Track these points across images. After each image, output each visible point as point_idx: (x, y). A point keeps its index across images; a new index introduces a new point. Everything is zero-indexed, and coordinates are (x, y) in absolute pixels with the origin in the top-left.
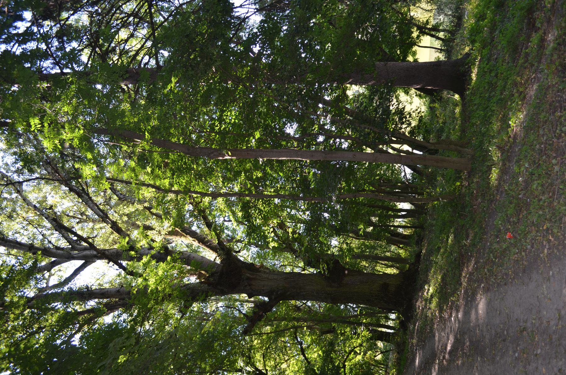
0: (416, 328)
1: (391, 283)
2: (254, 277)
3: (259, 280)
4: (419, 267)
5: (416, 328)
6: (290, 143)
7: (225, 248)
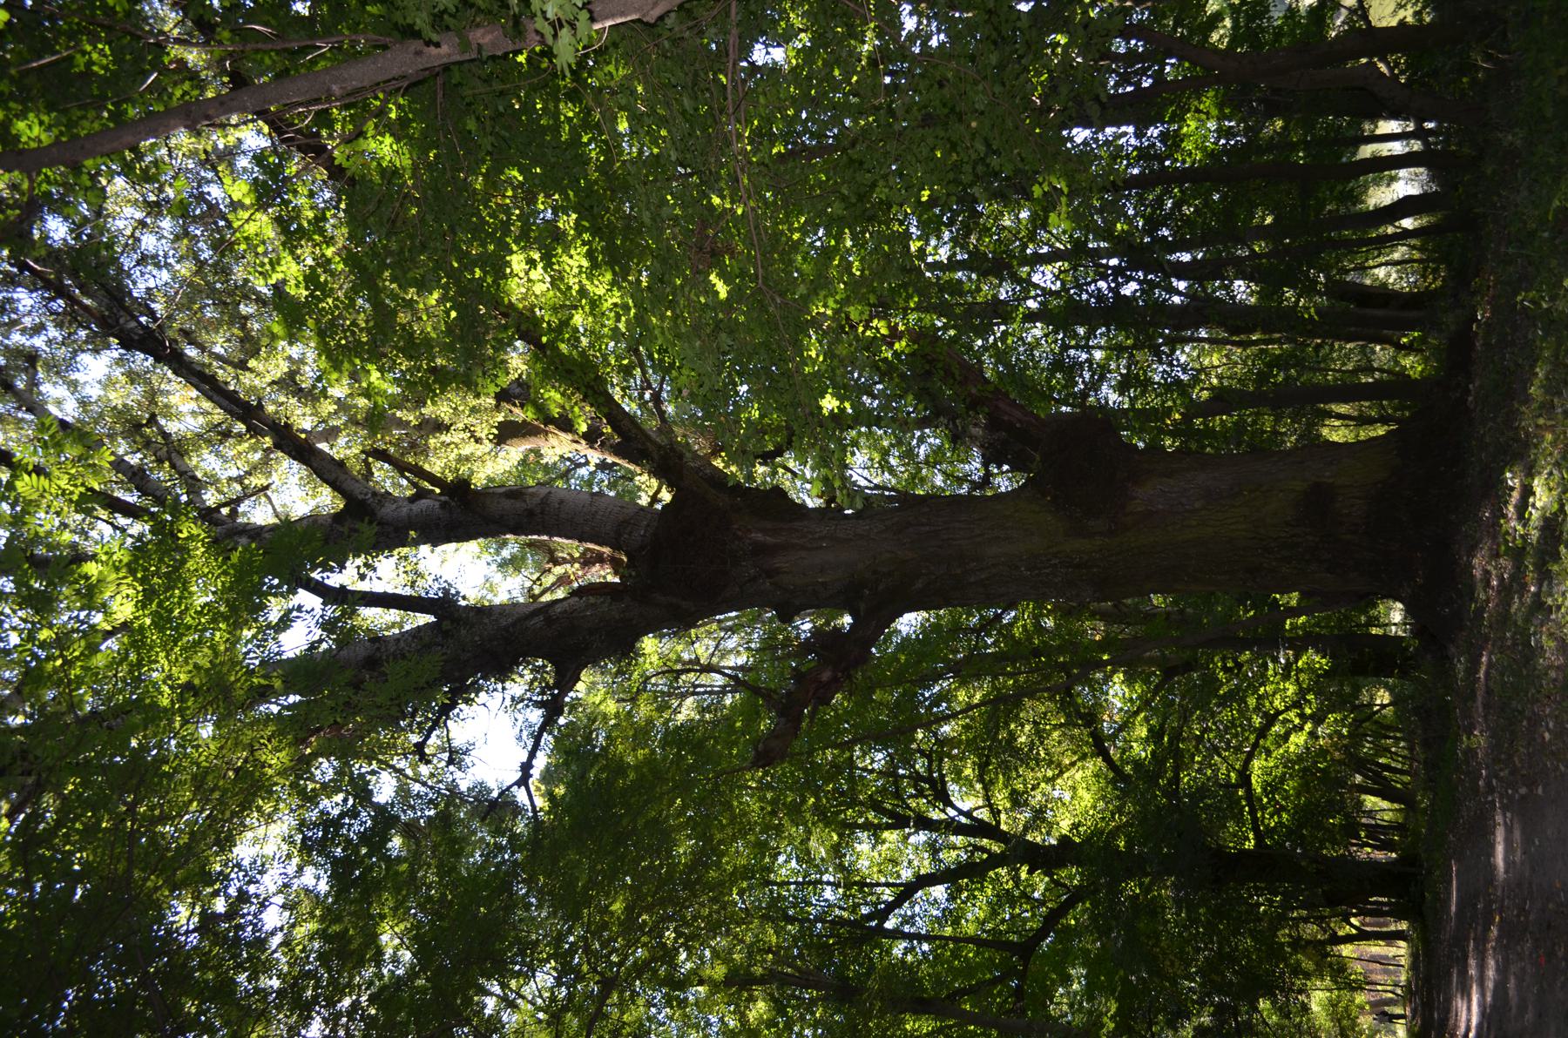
0: (1482, 675)
4: (1468, 392)
5: (1482, 675)
6: (155, 552)
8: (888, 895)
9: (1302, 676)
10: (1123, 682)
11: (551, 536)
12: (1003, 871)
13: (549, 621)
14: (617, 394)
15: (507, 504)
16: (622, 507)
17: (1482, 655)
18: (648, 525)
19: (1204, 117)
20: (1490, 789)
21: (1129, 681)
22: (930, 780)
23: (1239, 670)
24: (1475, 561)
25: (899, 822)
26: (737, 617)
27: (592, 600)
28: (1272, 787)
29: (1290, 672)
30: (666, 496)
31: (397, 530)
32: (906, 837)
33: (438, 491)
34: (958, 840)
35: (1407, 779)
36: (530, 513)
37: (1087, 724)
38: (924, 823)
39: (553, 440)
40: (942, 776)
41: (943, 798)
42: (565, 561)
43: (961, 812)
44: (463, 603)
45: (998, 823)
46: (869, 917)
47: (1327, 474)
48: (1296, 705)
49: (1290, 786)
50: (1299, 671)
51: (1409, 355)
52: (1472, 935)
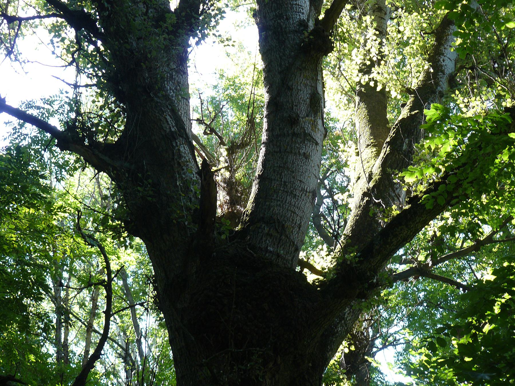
11: (267, 144)
15: (304, 95)
16: (300, 226)
18: (278, 255)
26: (225, 380)
27: (195, 188)
33: (321, 17)
36: (294, 121)
39: (368, 153)
44: (192, 41)
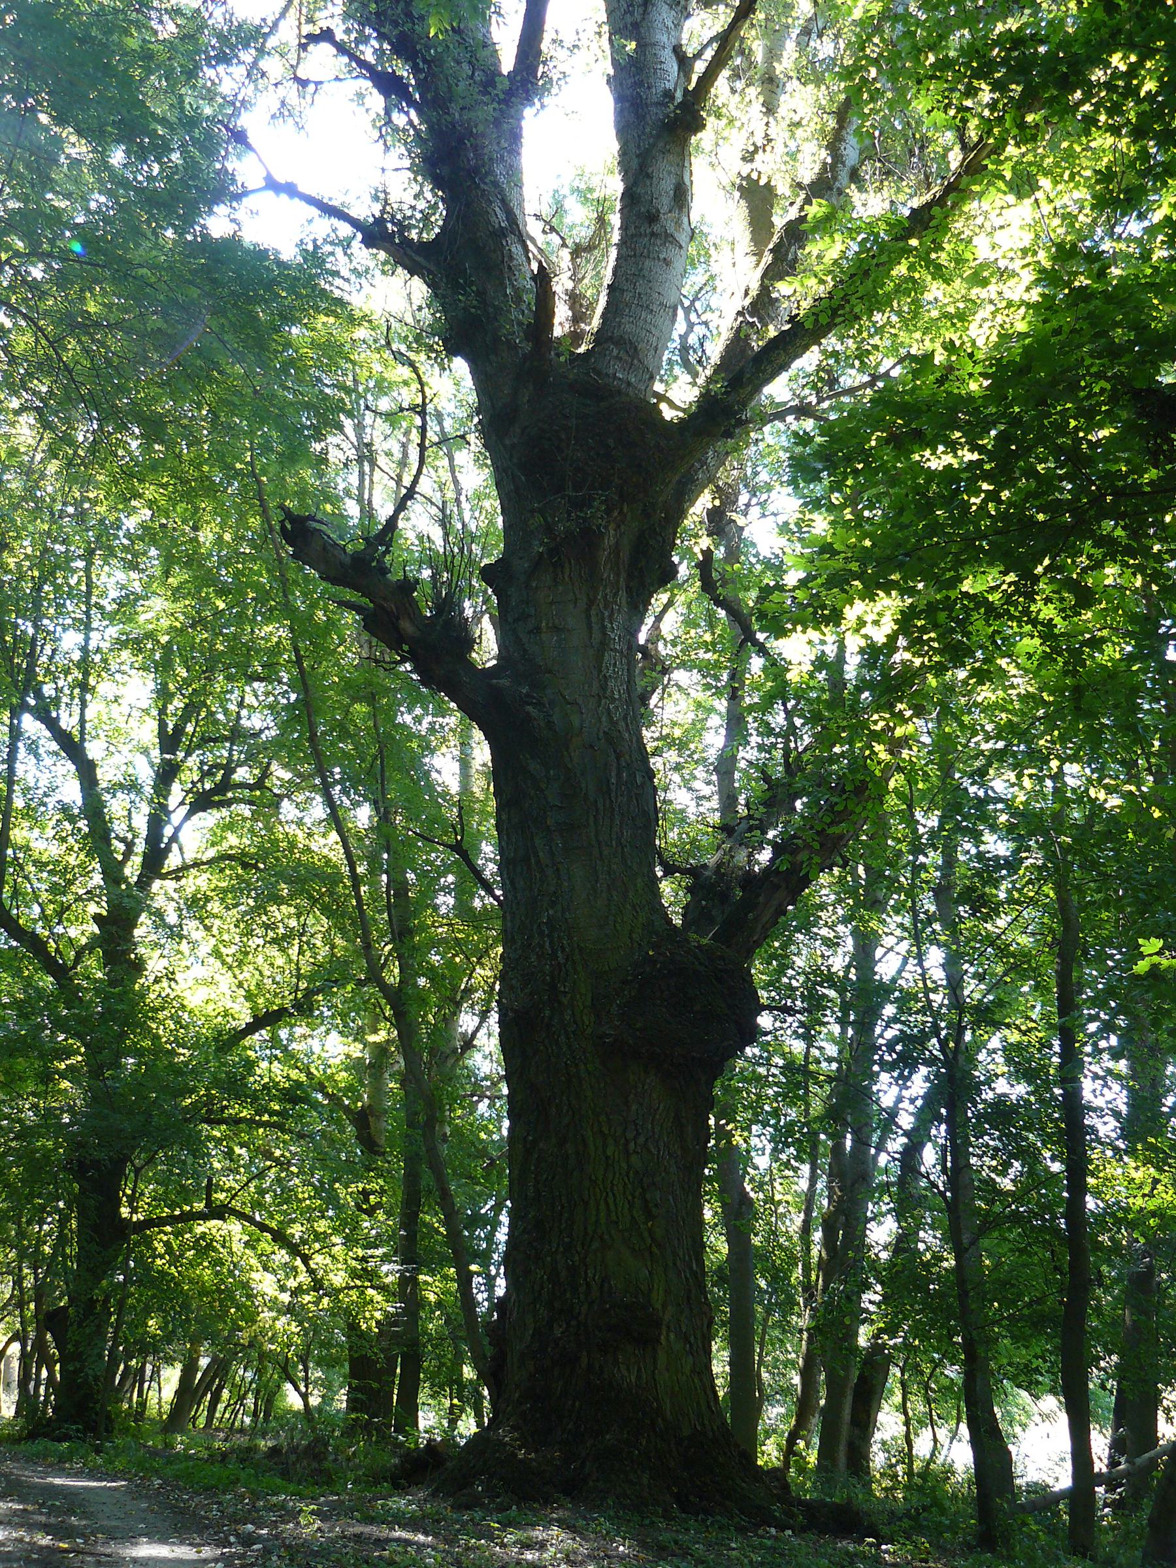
0: (398, 1533)
1: (662, 1357)
2: (606, 573)
3: (591, 602)
4: (782, 1529)
5: (398, 1533)
7: (743, 393)
8: (68, 721)
9: (354, 1294)
10: (348, 1056)
12: (97, 879)
13: (501, 233)
14: (831, 342)
16: (656, 349)
17: (426, 1534)
18: (629, 384)
19: (1147, 1190)
20: (247, 1541)
21: (354, 1066)
22: (225, 785)
23: (365, 1212)
24: (555, 1531)
25: (169, 741)
28: (204, 1247)
29: (359, 1278)
30: (668, 414)
31: (636, 25)
32: (145, 752)
34: (141, 823)
35: (201, 1422)
36: (653, 218)
37: (297, 1005)
38: (166, 774)
40: (228, 803)
41: (201, 802)
42: (576, 268)
43: (177, 829)
45: (164, 877)
46: (39, 695)
47: (672, 1336)
48: (318, 1285)
49: (206, 1274)
50: (362, 1290)
51: (780, 1449)
52: (30, 1508)
